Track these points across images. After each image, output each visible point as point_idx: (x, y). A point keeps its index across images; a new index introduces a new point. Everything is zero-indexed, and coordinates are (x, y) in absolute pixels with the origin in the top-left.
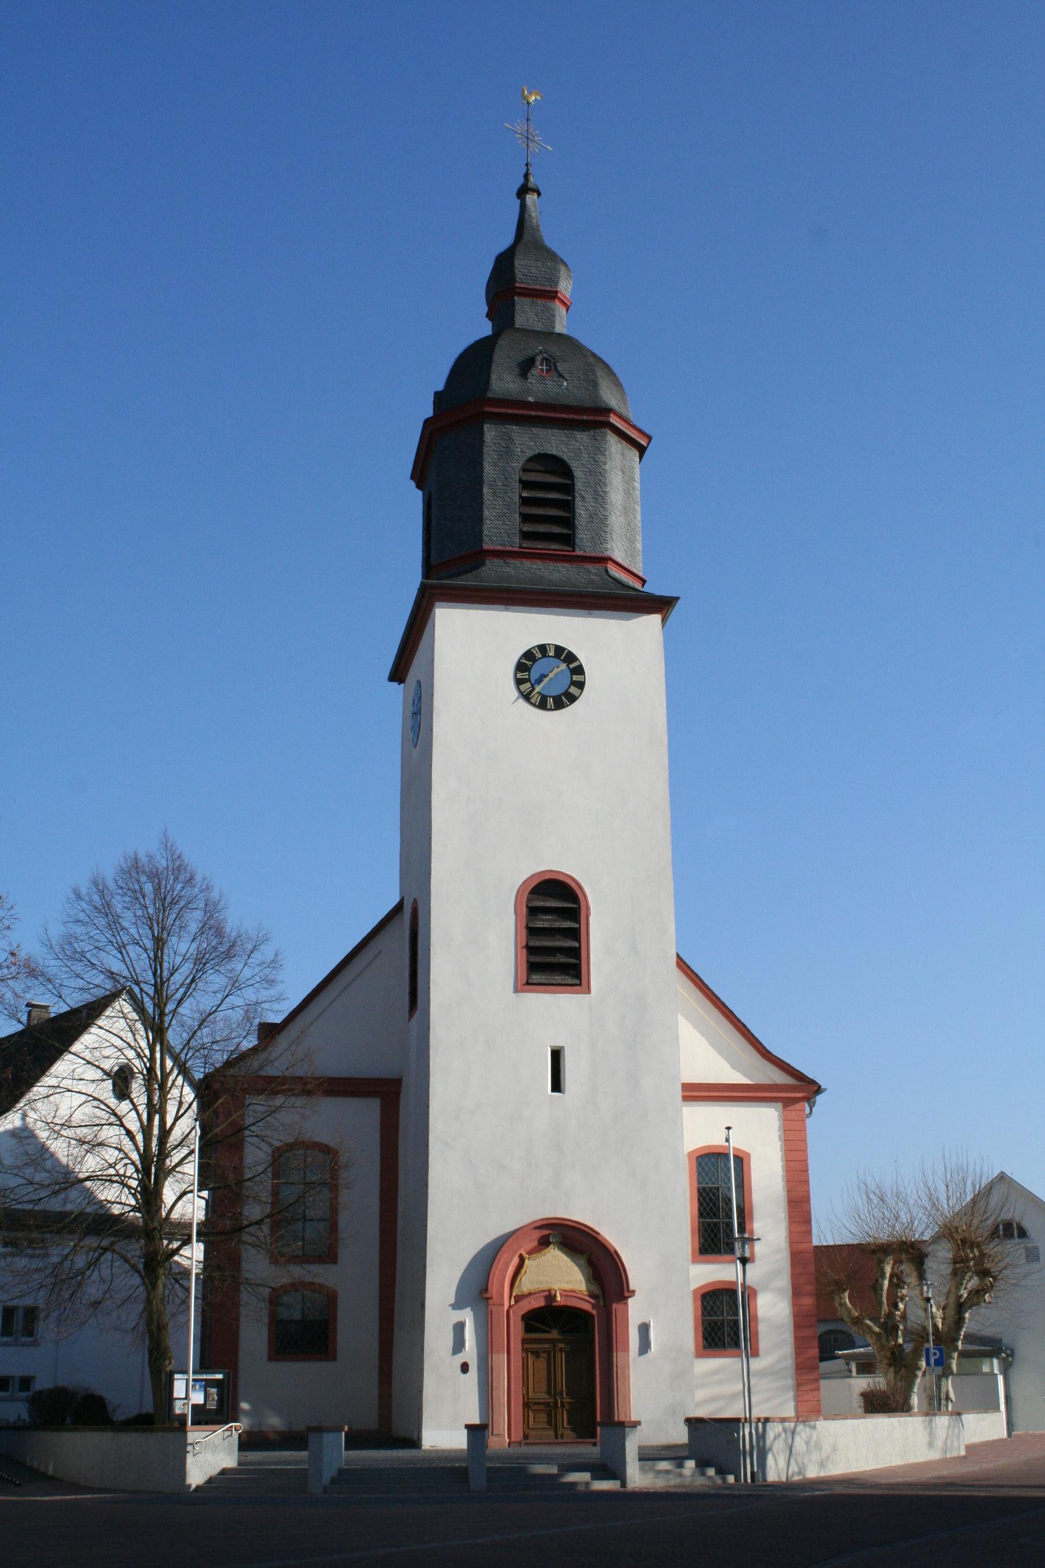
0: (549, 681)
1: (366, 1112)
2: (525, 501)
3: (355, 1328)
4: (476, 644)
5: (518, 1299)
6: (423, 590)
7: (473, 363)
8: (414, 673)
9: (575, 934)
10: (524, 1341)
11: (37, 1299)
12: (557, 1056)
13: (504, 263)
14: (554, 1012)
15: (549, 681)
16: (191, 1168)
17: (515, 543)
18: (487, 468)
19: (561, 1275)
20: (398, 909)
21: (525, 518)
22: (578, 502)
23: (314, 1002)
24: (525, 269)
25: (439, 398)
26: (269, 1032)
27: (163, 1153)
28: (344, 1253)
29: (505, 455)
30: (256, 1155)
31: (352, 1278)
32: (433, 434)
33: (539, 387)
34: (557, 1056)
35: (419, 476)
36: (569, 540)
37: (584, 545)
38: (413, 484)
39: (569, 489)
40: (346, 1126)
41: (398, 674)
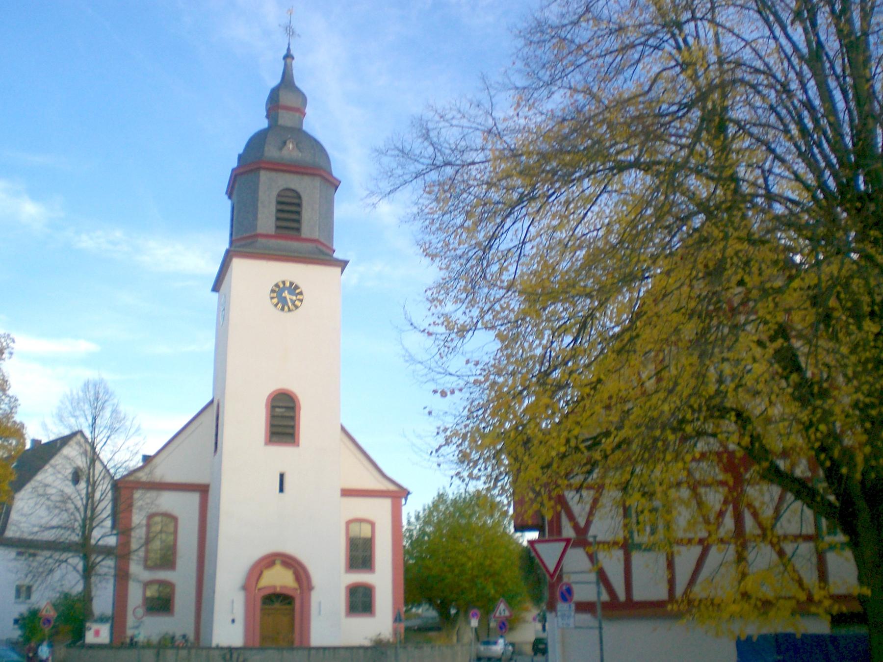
0: (286, 296)
1: (194, 498)
2: (279, 211)
3: (184, 599)
4: (255, 276)
5: (260, 589)
6: (228, 252)
7: (257, 142)
8: (223, 288)
9: (293, 418)
10: (262, 610)
11: (27, 582)
12: (282, 476)
13: (275, 94)
14: (282, 456)
15: (286, 296)
16: (108, 523)
17: (272, 230)
18: (260, 194)
19: (279, 578)
20: (212, 402)
21: (278, 219)
22: (304, 212)
23: (223, 278)
24: (286, 98)
25: (240, 157)
26: (147, 459)
27: (92, 519)
28: (180, 562)
29: (270, 186)
30: (138, 518)
31: (182, 577)
32: (236, 177)
33: (290, 151)
34: (282, 476)
35: (230, 193)
36: (298, 230)
37: (306, 231)
38: (226, 197)
39: (299, 205)
40: (183, 506)
41: (216, 288)
